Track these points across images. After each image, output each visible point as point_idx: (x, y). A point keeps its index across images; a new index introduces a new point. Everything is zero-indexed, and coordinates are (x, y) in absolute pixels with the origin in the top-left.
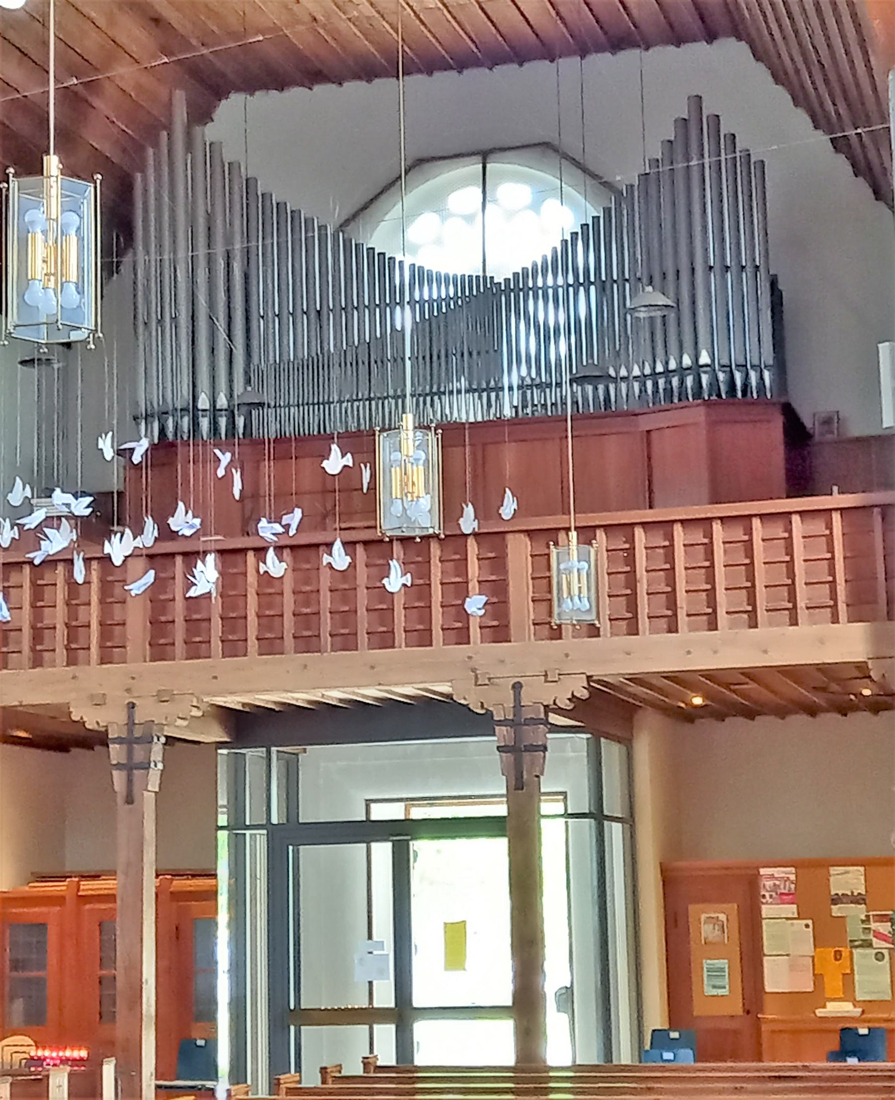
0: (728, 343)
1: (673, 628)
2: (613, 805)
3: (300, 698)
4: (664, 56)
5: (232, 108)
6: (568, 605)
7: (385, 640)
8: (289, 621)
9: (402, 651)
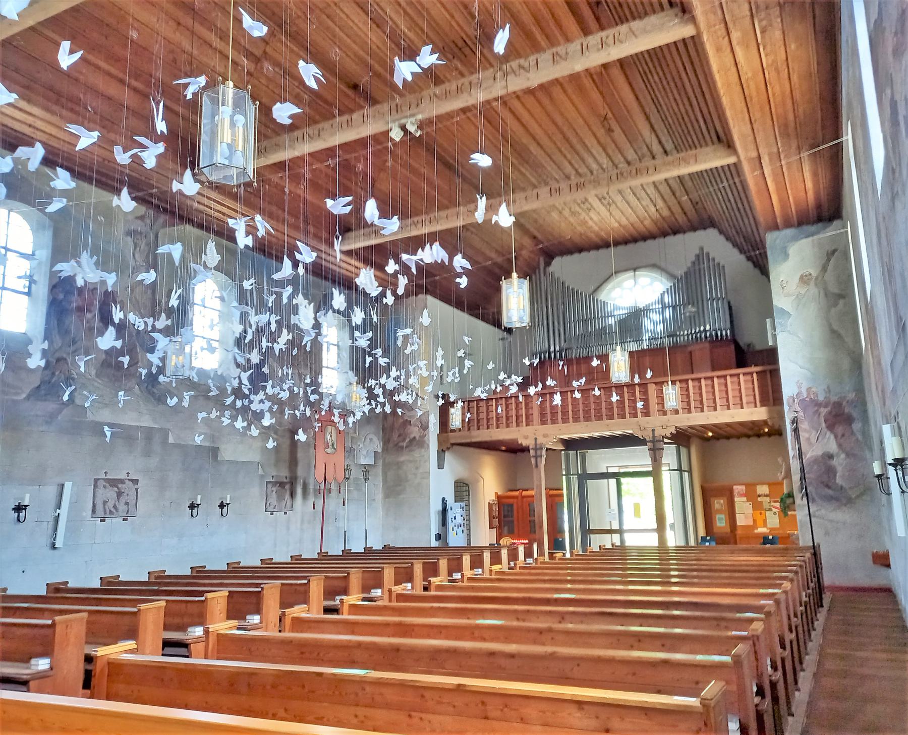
0: (714, 323)
1: (702, 411)
2: (685, 466)
3: (585, 435)
4: (690, 237)
5: (557, 262)
6: (669, 404)
7: (611, 417)
8: (593, 412)
9: (617, 420)
